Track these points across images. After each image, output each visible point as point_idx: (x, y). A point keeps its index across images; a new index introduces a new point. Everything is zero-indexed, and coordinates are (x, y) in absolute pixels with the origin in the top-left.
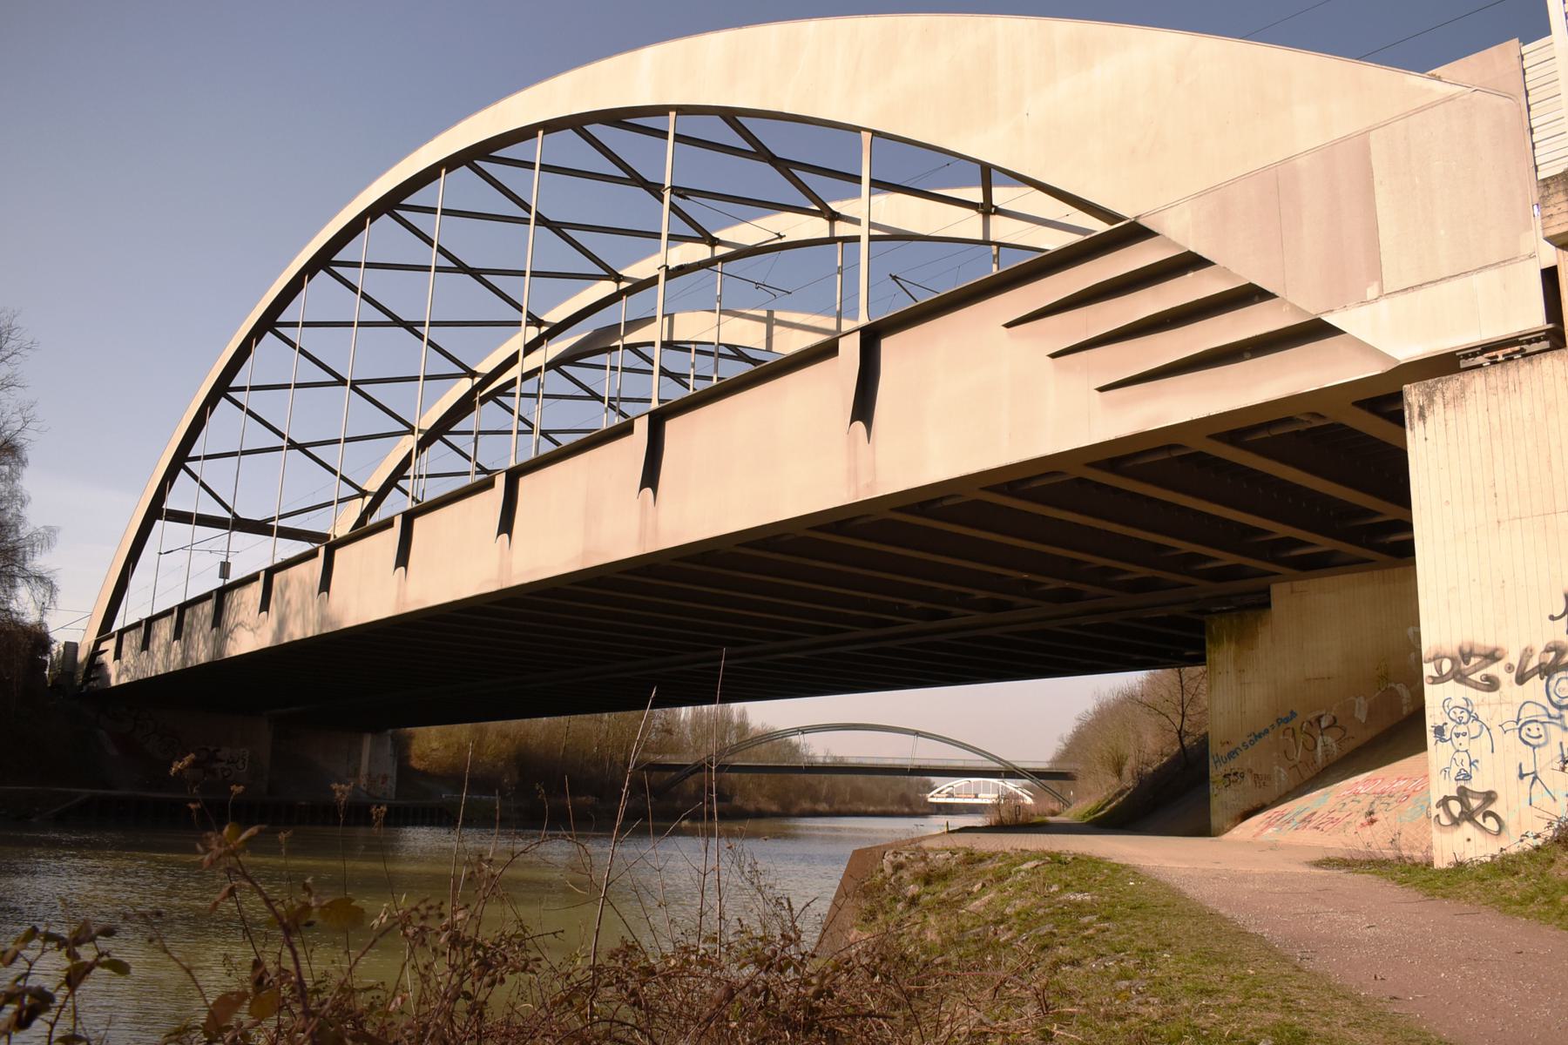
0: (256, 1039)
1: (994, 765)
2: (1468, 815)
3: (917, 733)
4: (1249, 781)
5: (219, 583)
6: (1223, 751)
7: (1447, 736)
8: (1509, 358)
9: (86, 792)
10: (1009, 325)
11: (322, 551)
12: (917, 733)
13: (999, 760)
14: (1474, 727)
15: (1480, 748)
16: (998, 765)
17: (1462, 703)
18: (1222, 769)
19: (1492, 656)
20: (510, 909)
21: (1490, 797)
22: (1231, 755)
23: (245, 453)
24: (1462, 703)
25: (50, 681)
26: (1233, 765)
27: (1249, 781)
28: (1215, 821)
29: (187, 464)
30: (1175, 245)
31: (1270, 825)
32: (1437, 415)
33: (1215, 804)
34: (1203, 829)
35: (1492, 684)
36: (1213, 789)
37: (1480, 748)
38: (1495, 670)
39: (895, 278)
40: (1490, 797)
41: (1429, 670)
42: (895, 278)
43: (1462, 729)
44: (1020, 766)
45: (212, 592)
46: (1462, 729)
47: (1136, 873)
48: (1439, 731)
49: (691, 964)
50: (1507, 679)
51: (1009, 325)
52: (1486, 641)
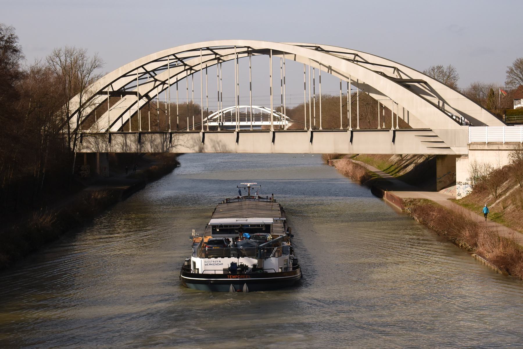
2: (459, 195)
4: (443, 182)
6: (439, 177)
15: (460, 190)
18: (439, 180)
19: (461, 183)
20: (255, 204)
21: (461, 194)
22: (440, 178)
23: (186, 77)
25: (383, 191)
26: (441, 180)
27: (443, 182)
28: (438, 189)
31: (445, 191)
32: (458, 161)
33: (437, 186)
34: (435, 190)
35: (461, 185)
36: (437, 184)
37: (460, 190)
38: (461, 184)
40: (461, 194)
41: (457, 183)
47: (431, 201)
50: (462, 185)
52: (461, 181)
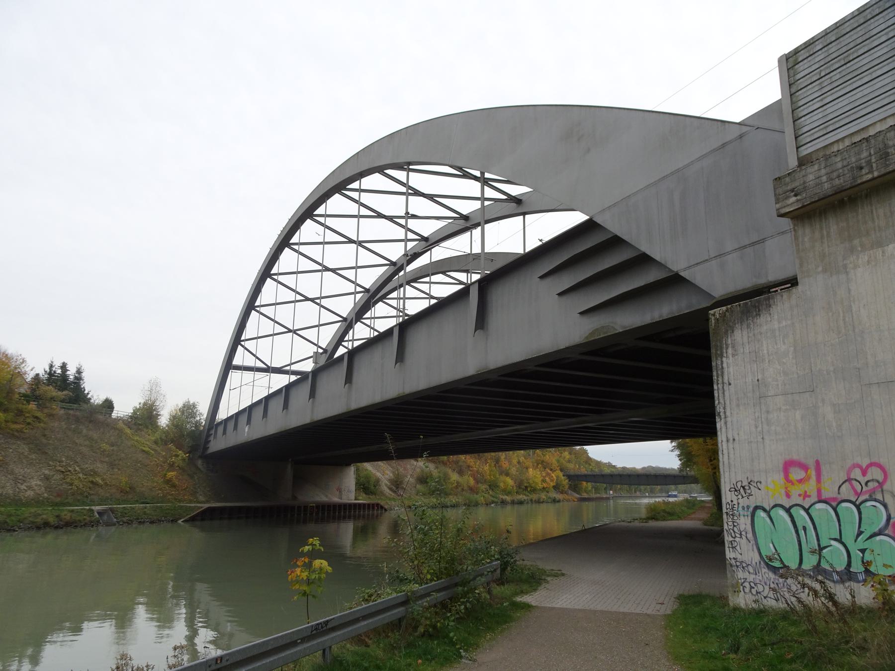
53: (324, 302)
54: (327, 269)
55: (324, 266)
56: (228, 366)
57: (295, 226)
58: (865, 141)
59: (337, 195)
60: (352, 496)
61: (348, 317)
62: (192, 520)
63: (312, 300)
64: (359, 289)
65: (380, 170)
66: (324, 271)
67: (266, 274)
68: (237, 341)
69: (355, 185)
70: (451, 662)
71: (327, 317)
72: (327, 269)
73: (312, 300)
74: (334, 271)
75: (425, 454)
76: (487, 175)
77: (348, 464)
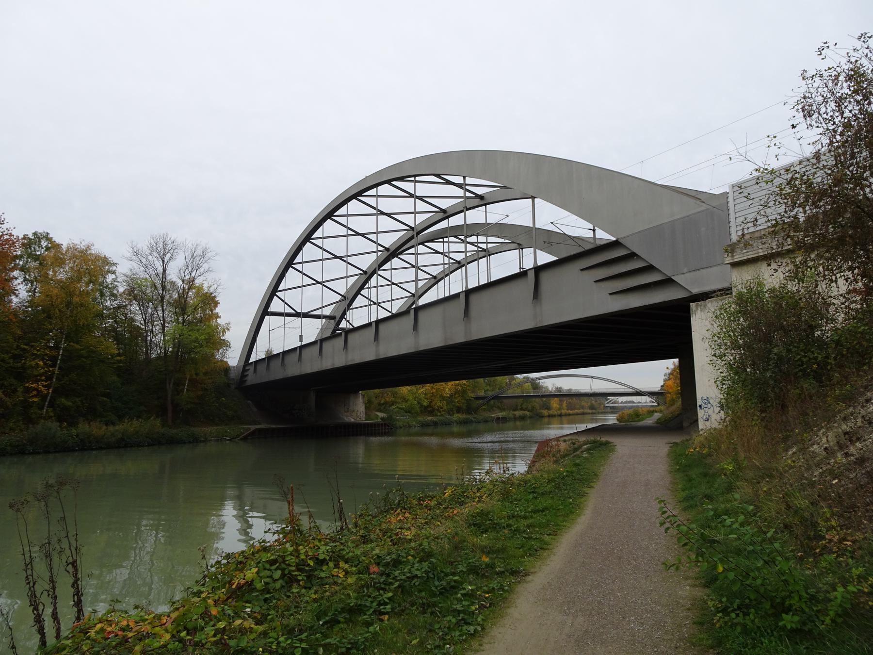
0: (769, 404)
1: (630, 390)
3: (592, 377)
5: (299, 344)
7: (702, 408)
8: (722, 295)
9: (253, 427)
10: (581, 270)
11: (343, 334)
12: (592, 377)
13: (633, 388)
14: (709, 405)
16: (632, 390)
17: (706, 398)
24: (706, 398)
29: (277, 293)
30: (630, 250)
39: (552, 223)
42: (552, 223)
43: (706, 406)
44: (643, 390)
45: (296, 348)
46: (706, 406)
48: (700, 406)
49: (721, 560)
51: (581, 270)
53: (350, 259)
54: (383, 213)
55: (379, 210)
56: (265, 312)
57: (318, 224)
58: (63, 516)
59: (354, 200)
60: (363, 415)
61: (447, 210)
62: (245, 439)
63: (340, 258)
64: (380, 248)
65: (389, 182)
66: (379, 214)
67: (307, 238)
68: (274, 291)
69: (373, 192)
70: (364, 553)
71: (353, 271)
72: (383, 213)
73: (340, 258)
74: (336, 257)
75: (652, 286)
76: (469, 180)
77: (356, 392)
